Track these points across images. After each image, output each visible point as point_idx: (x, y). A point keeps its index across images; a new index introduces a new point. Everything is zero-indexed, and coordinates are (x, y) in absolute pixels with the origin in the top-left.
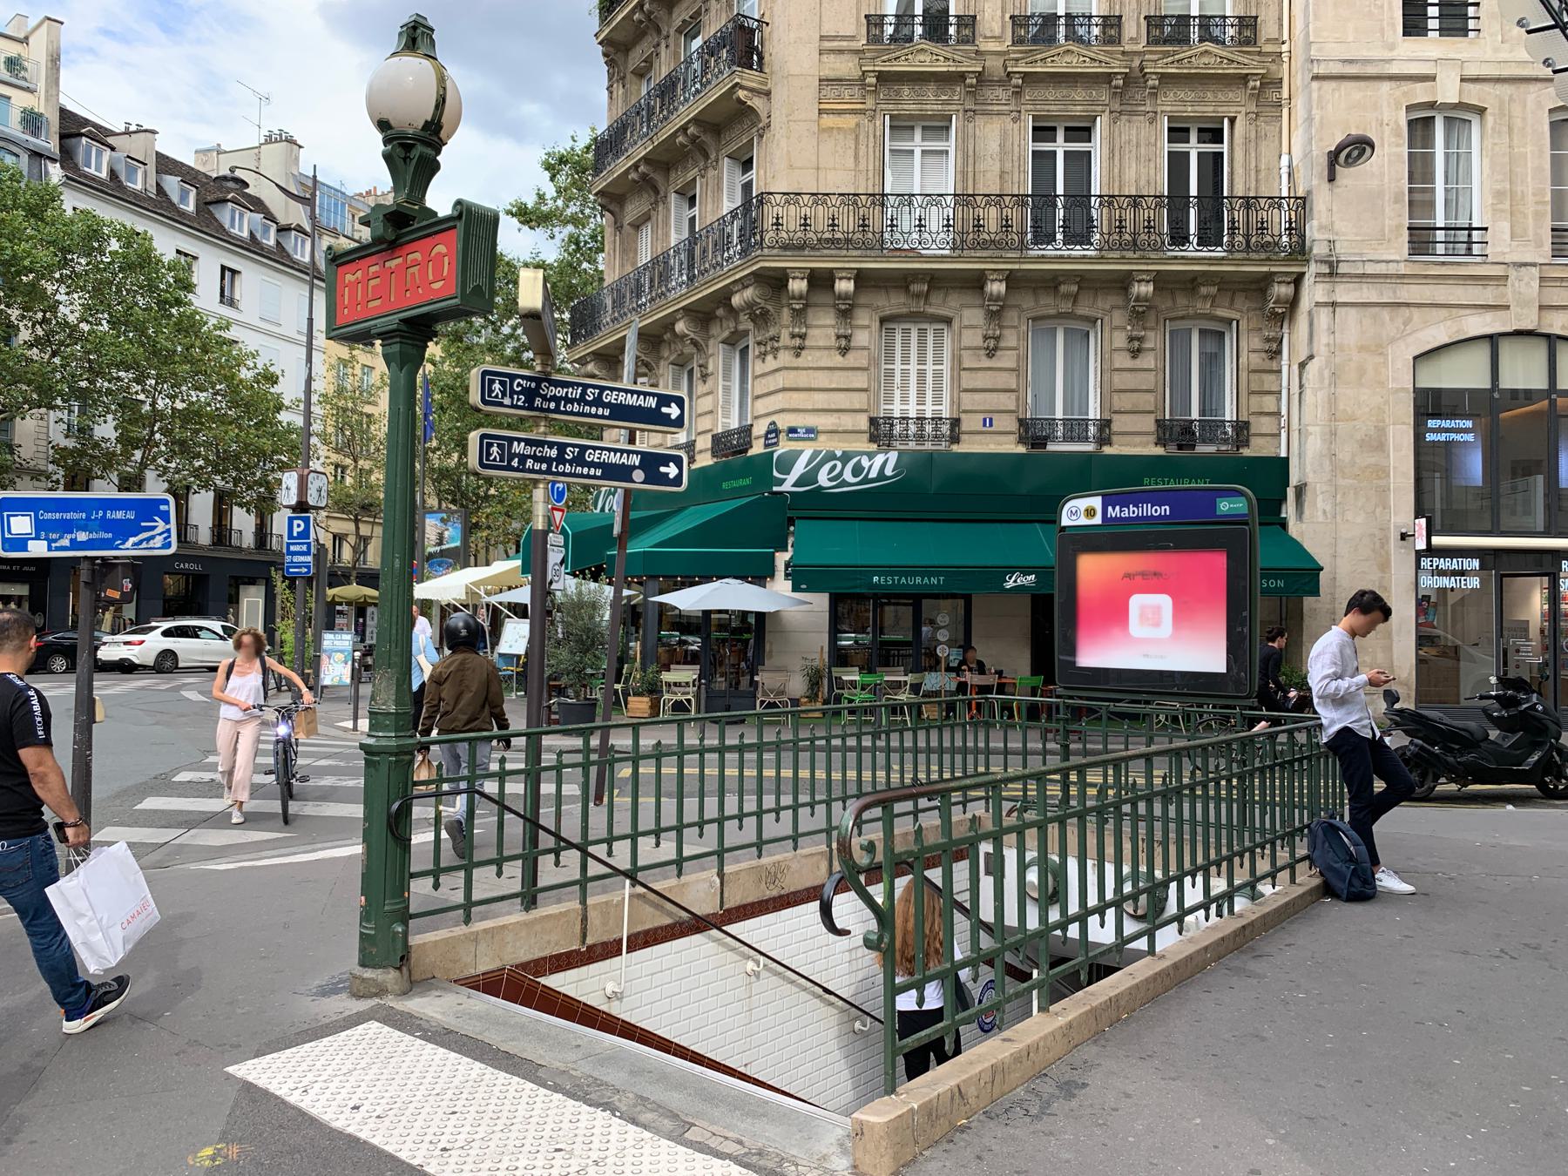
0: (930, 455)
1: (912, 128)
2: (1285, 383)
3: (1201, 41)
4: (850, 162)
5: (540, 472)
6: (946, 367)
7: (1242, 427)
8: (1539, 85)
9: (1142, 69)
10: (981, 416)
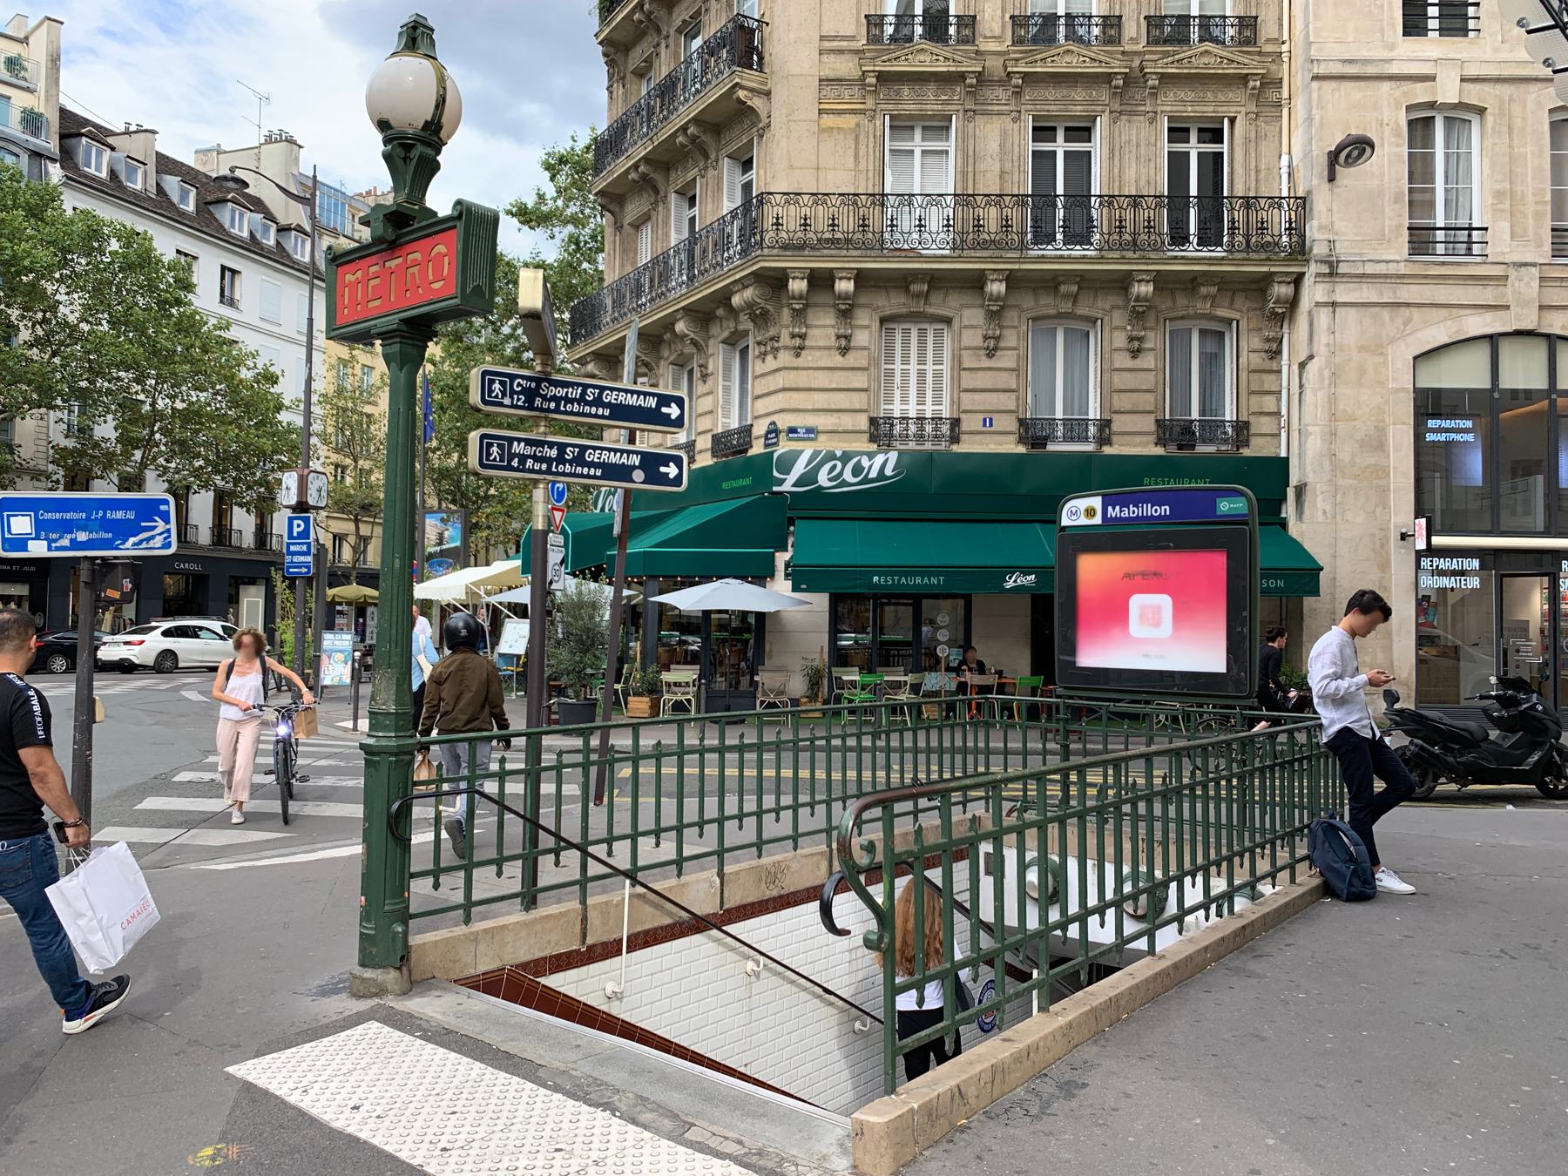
0: (930, 455)
1: (912, 128)
2: (1285, 383)
3: (1201, 41)
4: (850, 162)
5: (540, 472)
6: (946, 367)
7: (1242, 427)
8: (1539, 85)
9: (1142, 69)
10: (981, 416)
